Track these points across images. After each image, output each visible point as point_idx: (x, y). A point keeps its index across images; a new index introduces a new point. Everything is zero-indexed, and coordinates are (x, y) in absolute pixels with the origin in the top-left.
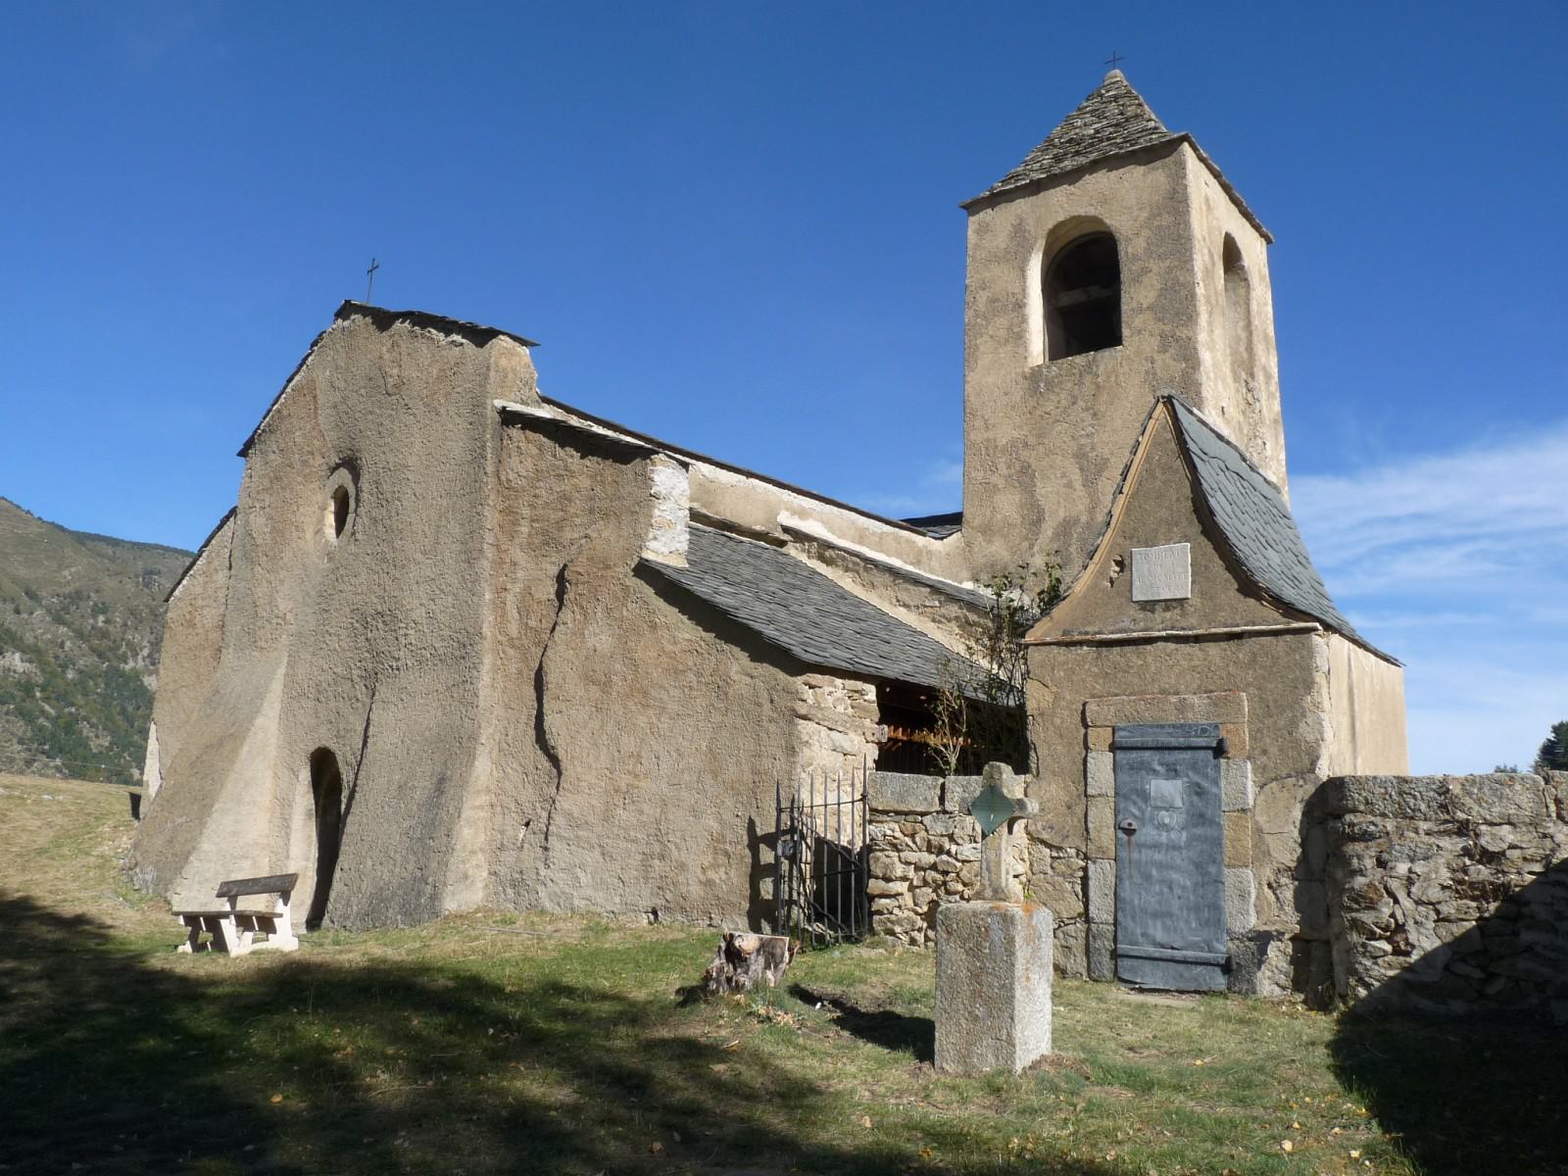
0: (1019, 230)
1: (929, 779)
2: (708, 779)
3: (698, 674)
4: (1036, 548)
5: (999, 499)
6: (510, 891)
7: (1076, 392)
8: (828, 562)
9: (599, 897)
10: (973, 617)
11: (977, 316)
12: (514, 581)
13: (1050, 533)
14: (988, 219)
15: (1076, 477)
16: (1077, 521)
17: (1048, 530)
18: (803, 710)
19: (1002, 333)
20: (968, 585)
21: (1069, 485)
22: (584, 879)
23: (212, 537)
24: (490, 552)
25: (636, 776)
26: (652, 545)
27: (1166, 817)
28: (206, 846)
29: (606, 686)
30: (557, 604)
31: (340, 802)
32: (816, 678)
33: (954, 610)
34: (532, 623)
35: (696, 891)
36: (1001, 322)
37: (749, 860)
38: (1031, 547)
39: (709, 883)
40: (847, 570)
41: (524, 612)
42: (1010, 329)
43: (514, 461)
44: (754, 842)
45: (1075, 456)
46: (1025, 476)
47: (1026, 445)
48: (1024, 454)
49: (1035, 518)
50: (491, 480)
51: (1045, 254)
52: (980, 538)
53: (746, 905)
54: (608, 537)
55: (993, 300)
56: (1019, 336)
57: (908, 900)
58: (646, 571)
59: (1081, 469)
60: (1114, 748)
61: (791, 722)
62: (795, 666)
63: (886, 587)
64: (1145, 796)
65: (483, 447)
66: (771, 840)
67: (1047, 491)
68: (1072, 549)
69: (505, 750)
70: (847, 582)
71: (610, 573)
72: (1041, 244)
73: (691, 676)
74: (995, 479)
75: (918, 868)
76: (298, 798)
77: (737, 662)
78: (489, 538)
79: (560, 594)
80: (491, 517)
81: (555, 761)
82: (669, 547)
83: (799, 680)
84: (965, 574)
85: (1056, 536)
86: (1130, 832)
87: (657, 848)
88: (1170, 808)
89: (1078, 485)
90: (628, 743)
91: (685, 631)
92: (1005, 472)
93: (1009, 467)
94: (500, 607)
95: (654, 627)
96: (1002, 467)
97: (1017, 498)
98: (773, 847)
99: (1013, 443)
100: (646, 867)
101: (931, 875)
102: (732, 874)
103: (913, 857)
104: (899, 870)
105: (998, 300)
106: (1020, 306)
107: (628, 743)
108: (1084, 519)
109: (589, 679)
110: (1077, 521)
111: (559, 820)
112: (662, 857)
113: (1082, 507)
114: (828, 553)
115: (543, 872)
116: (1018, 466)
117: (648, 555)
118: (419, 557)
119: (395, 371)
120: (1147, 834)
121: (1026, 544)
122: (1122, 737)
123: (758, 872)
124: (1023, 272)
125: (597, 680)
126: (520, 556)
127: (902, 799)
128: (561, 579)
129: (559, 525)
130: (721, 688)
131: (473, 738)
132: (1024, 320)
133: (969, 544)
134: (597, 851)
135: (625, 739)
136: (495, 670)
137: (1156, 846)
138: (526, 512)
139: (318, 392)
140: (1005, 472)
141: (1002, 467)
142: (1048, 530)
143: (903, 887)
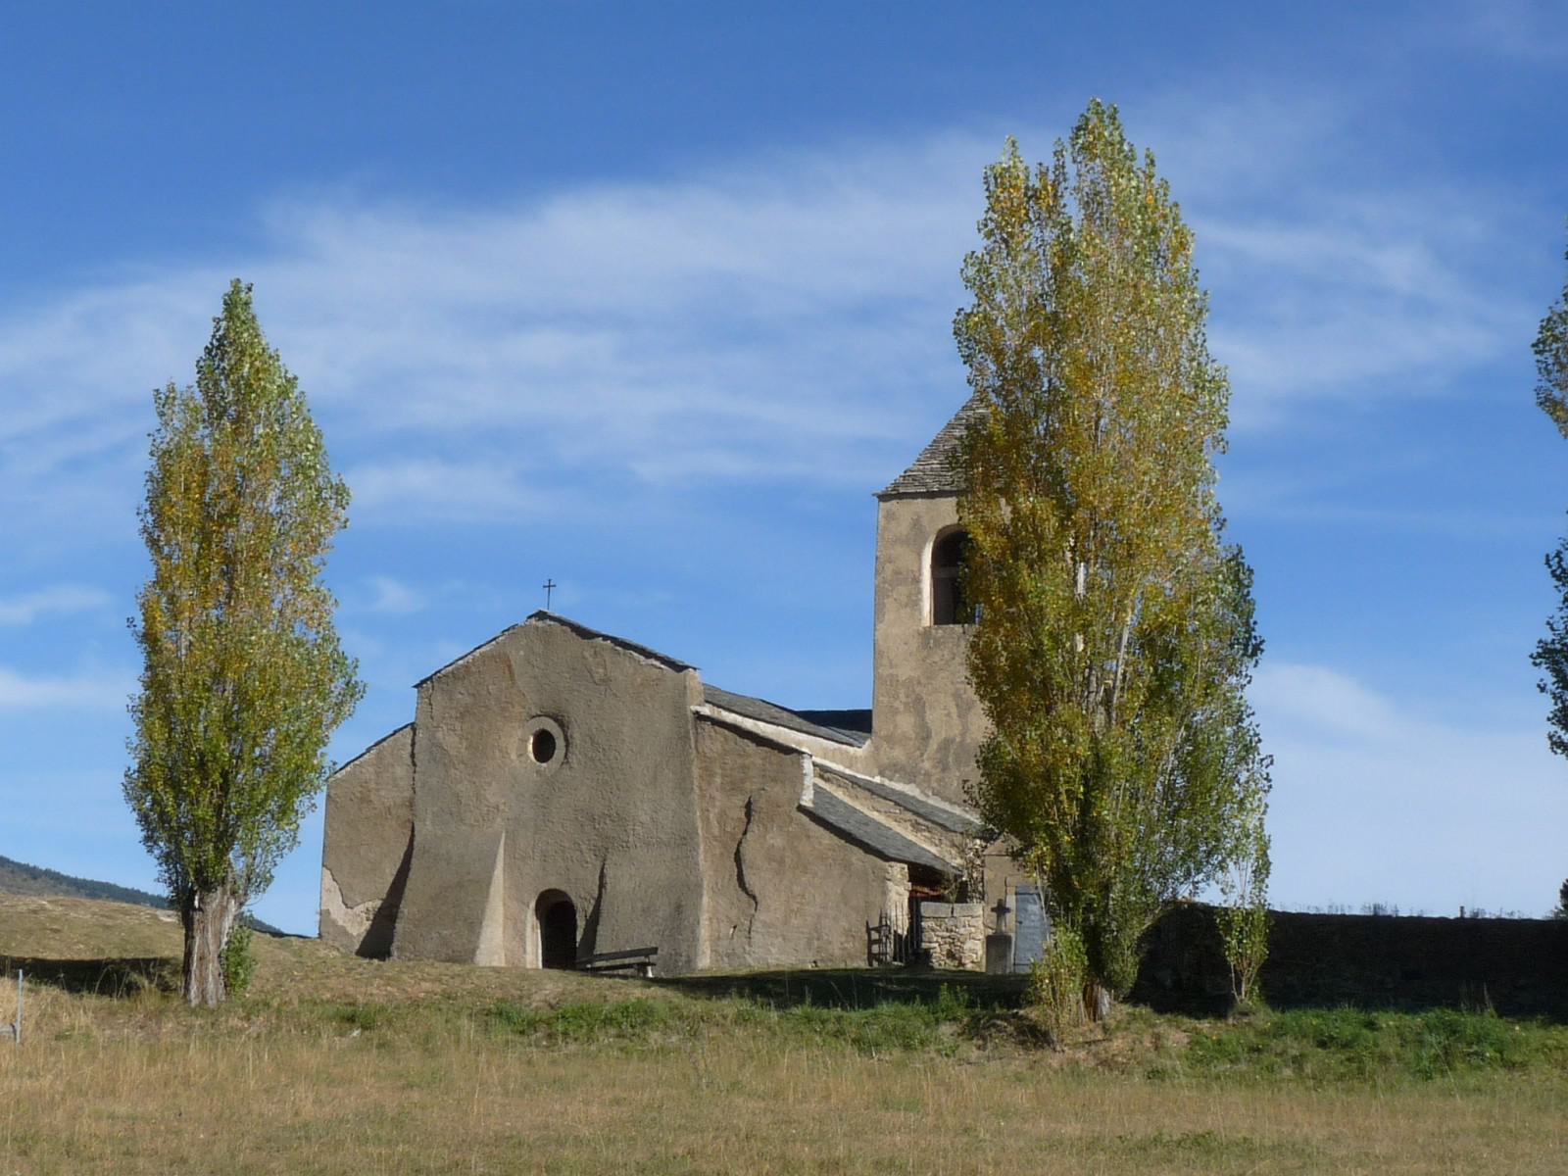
0: (916, 523)
1: (946, 905)
2: (842, 906)
3: (834, 860)
4: (925, 756)
5: (899, 719)
6: (726, 959)
7: (955, 651)
8: (827, 780)
9: (783, 958)
10: (921, 821)
11: (884, 582)
12: (714, 806)
13: (935, 747)
14: (894, 509)
15: (954, 710)
16: (953, 740)
17: (933, 745)
18: (888, 876)
19: (904, 599)
20: (877, 779)
21: (948, 715)
22: (774, 951)
23: (384, 740)
24: (697, 791)
25: (802, 904)
26: (804, 798)
27: (1033, 917)
28: (482, 946)
29: (781, 862)
30: (745, 820)
31: (574, 928)
32: (892, 863)
33: (909, 815)
34: (729, 829)
35: (837, 952)
36: (903, 590)
37: (866, 937)
38: (922, 755)
39: (845, 949)
40: (840, 786)
41: (722, 822)
42: (909, 596)
43: (708, 742)
44: (869, 930)
45: (953, 695)
46: (918, 706)
47: (919, 683)
48: (918, 689)
49: (925, 737)
50: (694, 751)
51: (935, 542)
52: (885, 745)
53: (866, 956)
54: (775, 791)
55: (897, 573)
56: (915, 603)
57: (938, 950)
58: (801, 809)
59: (957, 705)
60: (1016, 894)
61: (883, 882)
62: (887, 859)
63: (866, 799)
64: (1026, 910)
65: (688, 732)
66: (875, 929)
67: (932, 717)
68: (950, 759)
69: (716, 892)
70: (840, 794)
71: (780, 810)
72: (933, 538)
73: (830, 860)
74: (897, 704)
75: (942, 938)
76: (529, 918)
77: (856, 855)
78: (696, 783)
79: (748, 815)
80: (696, 771)
81: (754, 898)
82: (807, 799)
83: (887, 864)
84: (876, 771)
85: (939, 749)
86: (1021, 923)
87: (816, 935)
88: (1035, 914)
89: (955, 716)
90: (797, 889)
91: (827, 838)
92: (904, 700)
93: (907, 697)
94: (706, 820)
95: (808, 837)
96: (902, 696)
97: (913, 720)
98: (879, 932)
99: (910, 680)
100: (809, 943)
101: (948, 940)
102: (857, 944)
103: (940, 934)
104: (935, 939)
105: (901, 573)
106: (917, 581)
107: (797, 889)
108: (958, 740)
109: (770, 859)
110: (953, 740)
111: (757, 925)
112: (818, 939)
113: (957, 732)
114: (827, 775)
115: (747, 948)
116: (913, 697)
117: (803, 803)
118: (641, 787)
119: (601, 671)
120: (1026, 923)
121: (918, 753)
122: (1020, 890)
123: (871, 942)
124: (919, 554)
125: (777, 860)
126: (717, 795)
127: (936, 912)
128: (748, 806)
129: (743, 781)
130: (847, 866)
131: (699, 886)
132: (919, 592)
133: (877, 749)
134: (780, 939)
135: (795, 887)
136: (706, 852)
137: (1029, 927)
138: (719, 771)
139: (512, 663)
140: (904, 700)
141: (902, 696)
142: (933, 745)
143: (936, 945)
